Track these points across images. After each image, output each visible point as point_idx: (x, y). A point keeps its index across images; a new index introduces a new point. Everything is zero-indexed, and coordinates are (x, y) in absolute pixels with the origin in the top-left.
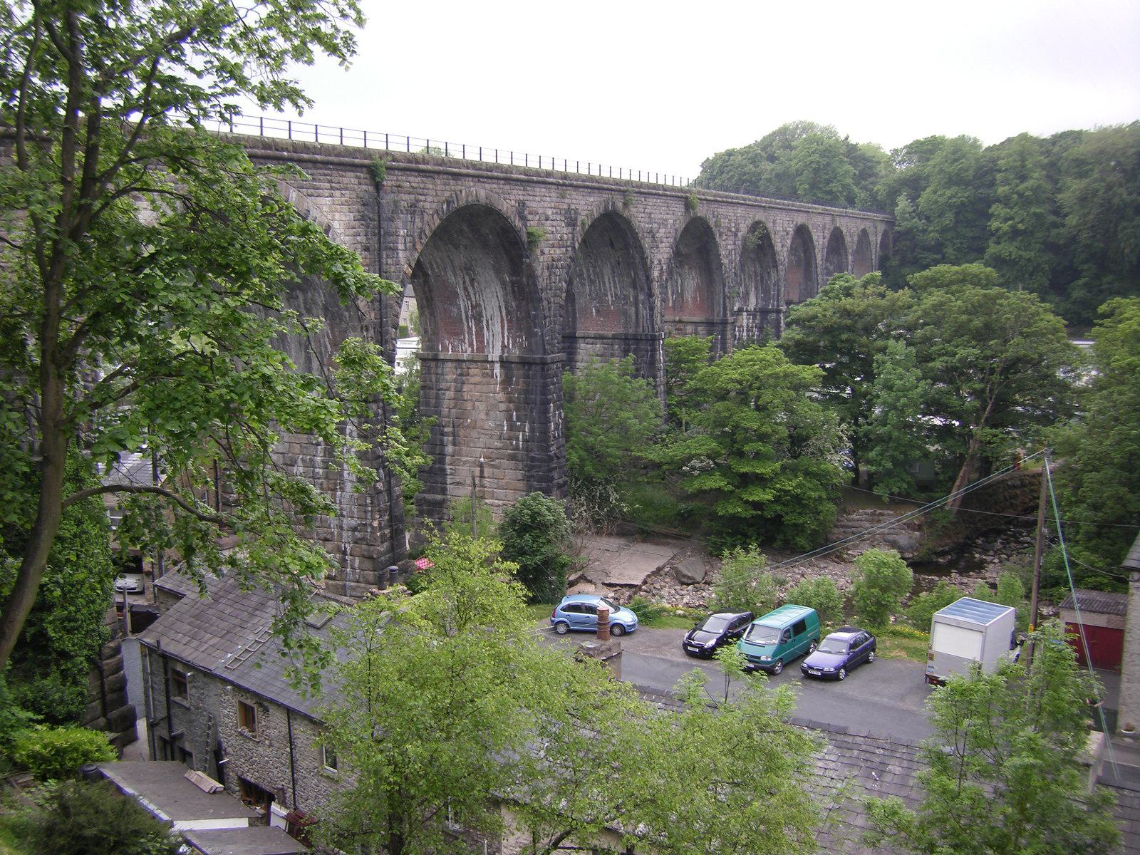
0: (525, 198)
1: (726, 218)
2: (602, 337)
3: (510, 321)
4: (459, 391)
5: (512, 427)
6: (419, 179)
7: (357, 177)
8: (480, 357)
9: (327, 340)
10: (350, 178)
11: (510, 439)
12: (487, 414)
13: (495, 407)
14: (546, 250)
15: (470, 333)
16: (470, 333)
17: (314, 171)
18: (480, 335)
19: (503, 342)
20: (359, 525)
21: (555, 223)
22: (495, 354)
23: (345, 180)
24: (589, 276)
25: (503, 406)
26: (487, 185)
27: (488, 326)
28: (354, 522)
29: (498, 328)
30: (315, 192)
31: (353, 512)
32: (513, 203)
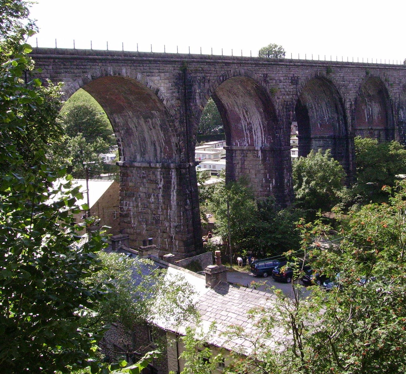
0: (267, 72)
1: (392, 76)
2: (323, 138)
3: (265, 131)
4: (243, 164)
5: (267, 181)
6: (207, 66)
7: (173, 67)
8: (251, 148)
9: (163, 141)
10: (169, 67)
11: (266, 187)
12: (255, 175)
13: (259, 171)
14: (281, 97)
15: (247, 137)
16: (247, 137)
17: (151, 65)
18: (252, 138)
19: (262, 141)
20: (177, 225)
21: (285, 84)
22: (258, 146)
23: (166, 68)
24: (315, 108)
25: (262, 172)
26: (245, 68)
27: (255, 133)
28: (176, 224)
29: (259, 134)
30: (151, 74)
31: (175, 219)
32: (260, 75)
